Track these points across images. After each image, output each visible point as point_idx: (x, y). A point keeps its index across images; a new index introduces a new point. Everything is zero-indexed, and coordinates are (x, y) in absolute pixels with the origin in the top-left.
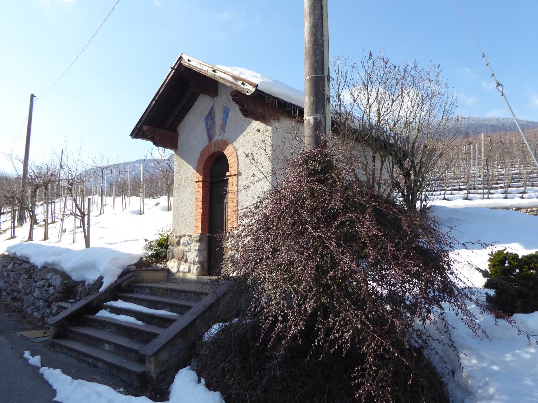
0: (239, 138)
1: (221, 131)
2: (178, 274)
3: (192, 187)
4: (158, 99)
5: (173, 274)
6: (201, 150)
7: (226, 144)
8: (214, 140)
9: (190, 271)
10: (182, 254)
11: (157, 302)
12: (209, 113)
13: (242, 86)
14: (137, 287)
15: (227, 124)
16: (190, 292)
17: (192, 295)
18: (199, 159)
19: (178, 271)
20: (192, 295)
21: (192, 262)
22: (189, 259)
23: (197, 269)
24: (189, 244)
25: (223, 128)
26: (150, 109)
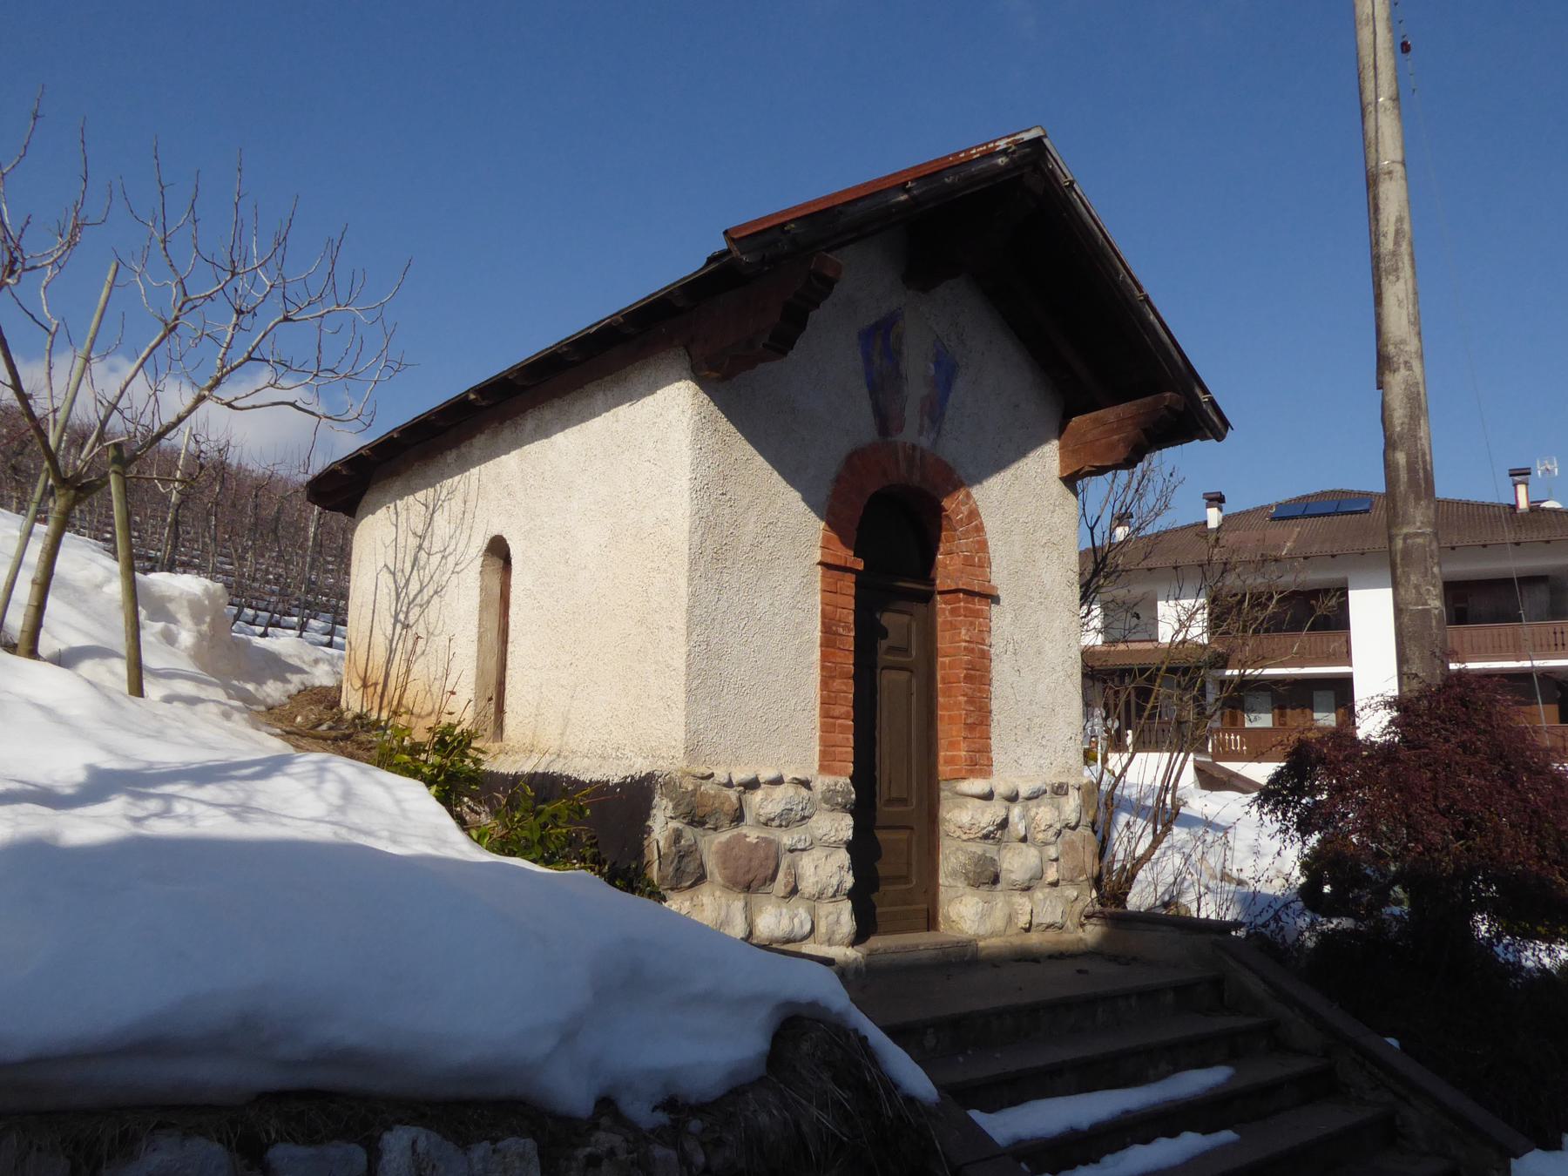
1: (927, 421)
21: (831, 891)
22: (808, 885)
25: (935, 412)
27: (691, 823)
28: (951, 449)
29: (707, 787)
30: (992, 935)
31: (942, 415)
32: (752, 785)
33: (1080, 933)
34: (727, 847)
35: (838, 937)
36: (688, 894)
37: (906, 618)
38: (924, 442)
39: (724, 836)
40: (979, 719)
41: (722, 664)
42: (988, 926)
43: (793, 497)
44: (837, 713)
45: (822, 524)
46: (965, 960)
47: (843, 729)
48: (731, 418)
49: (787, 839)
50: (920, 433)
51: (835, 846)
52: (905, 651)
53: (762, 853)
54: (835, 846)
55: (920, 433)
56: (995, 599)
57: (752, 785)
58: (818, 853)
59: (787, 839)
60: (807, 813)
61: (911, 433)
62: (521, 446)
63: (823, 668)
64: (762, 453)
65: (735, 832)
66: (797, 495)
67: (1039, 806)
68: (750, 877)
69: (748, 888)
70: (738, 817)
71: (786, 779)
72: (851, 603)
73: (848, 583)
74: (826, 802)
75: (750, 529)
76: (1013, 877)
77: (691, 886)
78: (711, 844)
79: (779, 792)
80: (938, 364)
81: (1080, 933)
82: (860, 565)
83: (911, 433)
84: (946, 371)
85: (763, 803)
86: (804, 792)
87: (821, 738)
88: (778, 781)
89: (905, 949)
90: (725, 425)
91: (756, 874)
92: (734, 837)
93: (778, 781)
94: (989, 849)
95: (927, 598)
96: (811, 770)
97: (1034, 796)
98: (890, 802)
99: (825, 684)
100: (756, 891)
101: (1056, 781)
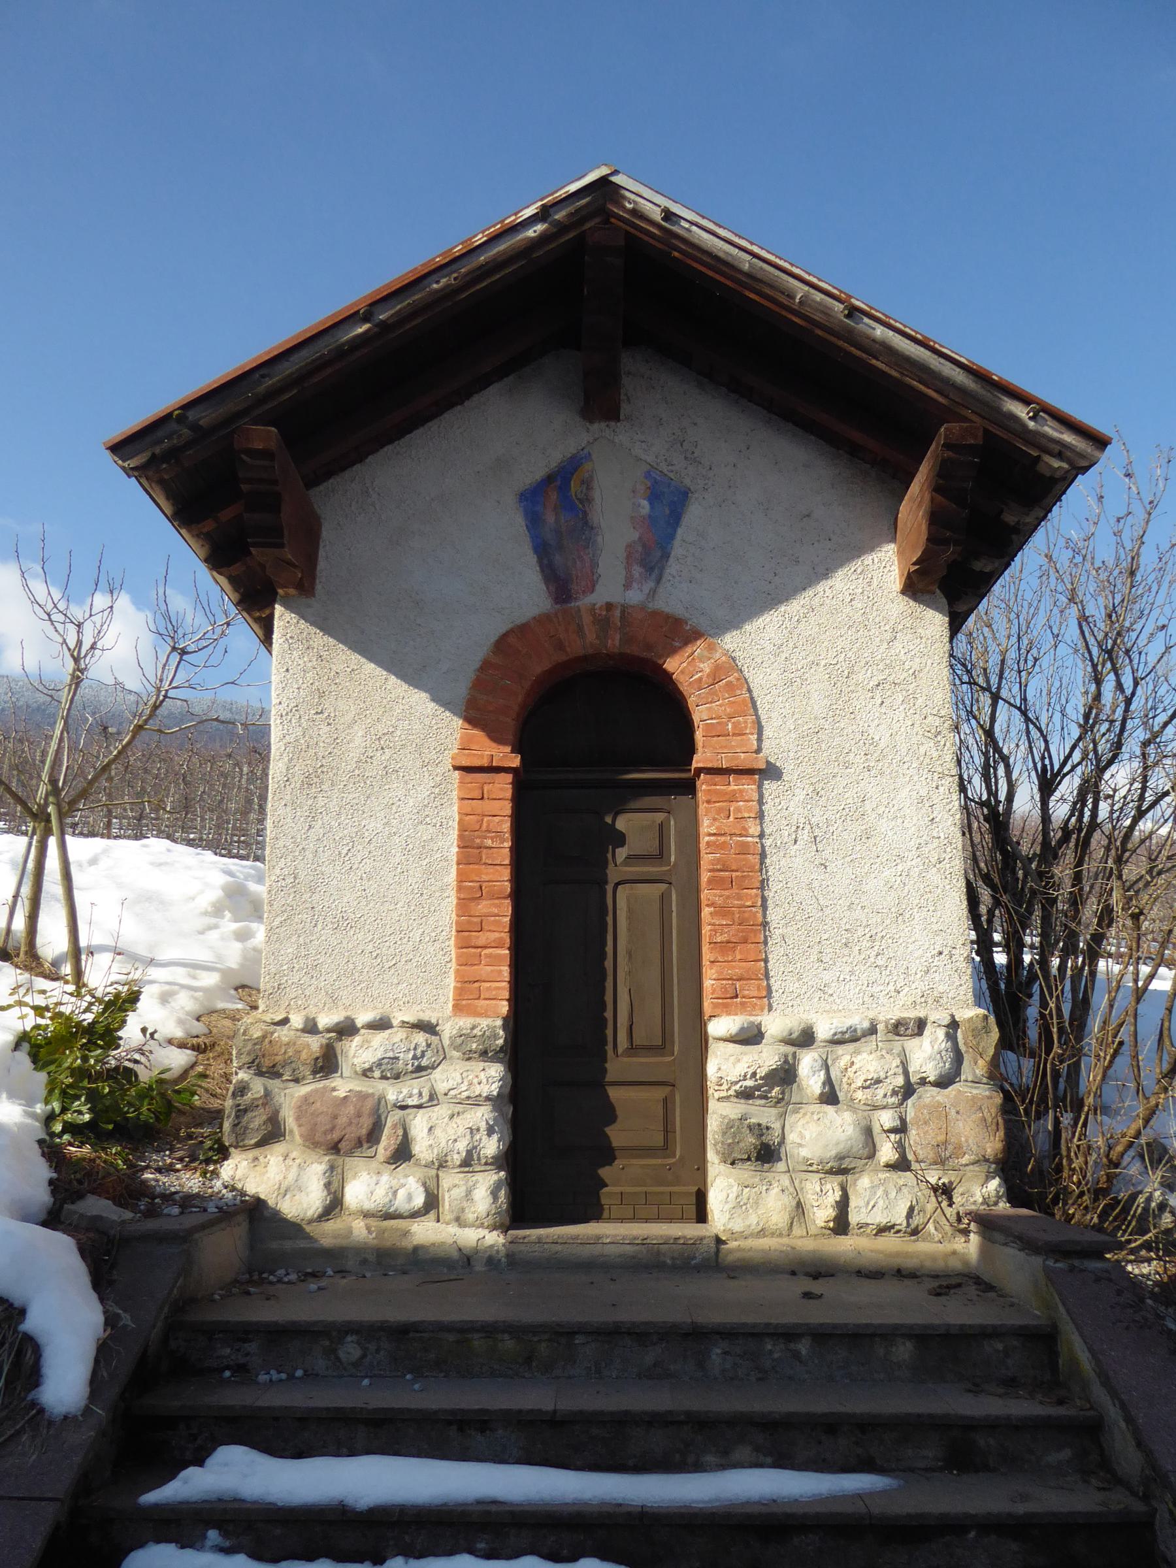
0: (760, 622)
1: (637, 570)
2: (330, 1226)
3: (423, 792)
4: (401, 320)
5: (293, 1229)
6: (497, 627)
7: (680, 633)
8: (585, 602)
9: (432, 1203)
10: (366, 1123)
11: (622, 1421)
12: (549, 479)
13: (1031, 424)
14: (243, 1333)
15: (677, 549)
16: (788, 1335)
17: (804, 1347)
18: (485, 666)
19: (334, 1205)
20: (804, 1347)
21: (457, 1159)
22: (422, 1147)
23: (494, 1194)
24: (420, 1069)
25: (651, 557)
26: (323, 348)
27: (260, 1073)
28: (675, 596)
29: (283, 1034)
30: (762, 1233)
31: (666, 556)
32: (346, 1029)
33: (959, 1244)
34: (306, 1100)
35: (471, 1217)
36: (251, 1154)
37: (660, 817)
38: (635, 597)
39: (303, 1090)
40: (752, 931)
41: (316, 897)
42: (753, 1220)
43: (419, 701)
44: (481, 942)
45: (458, 722)
46: (712, 1262)
47: (494, 961)
48: (326, 629)
49: (392, 1093)
50: (627, 586)
51: (474, 1101)
52: (661, 855)
53: (350, 1110)
54: (474, 1101)
55: (627, 586)
56: (771, 772)
57: (346, 1029)
58: (441, 1112)
59: (392, 1093)
60: (424, 1062)
61: (612, 585)
62: (681, 693)
63: (460, 889)
64: (371, 659)
65: (320, 1085)
66: (424, 696)
67: (857, 1052)
68: (336, 1136)
69: (335, 1148)
70: (327, 1064)
71: (395, 1022)
72: (507, 808)
73: (503, 786)
74: (457, 1048)
75: (358, 739)
76: (804, 1153)
77: (259, 1145)
78: (290, 1098)
79: (380, 1038)
80: (654, 496)
81: (959, 1244)
82: (515, 761)
83: (612, 585)
84: (668, 503)
85: (360, 1052)
86: (420, 1038)
87: (457, 972)
88: (381, 1025)
89: (644, 1242)
90: (320, 639)
91: (352, 1137)
92: (316, 1091)
93: (381, 1025)
94: (762, 1114)
95: (688, 788)
96: (438, 1006)
97: (847, 1038)
98: (633, 1049)
99: (464, 905)
100: (350, 1153)
101: (913, 1014)
